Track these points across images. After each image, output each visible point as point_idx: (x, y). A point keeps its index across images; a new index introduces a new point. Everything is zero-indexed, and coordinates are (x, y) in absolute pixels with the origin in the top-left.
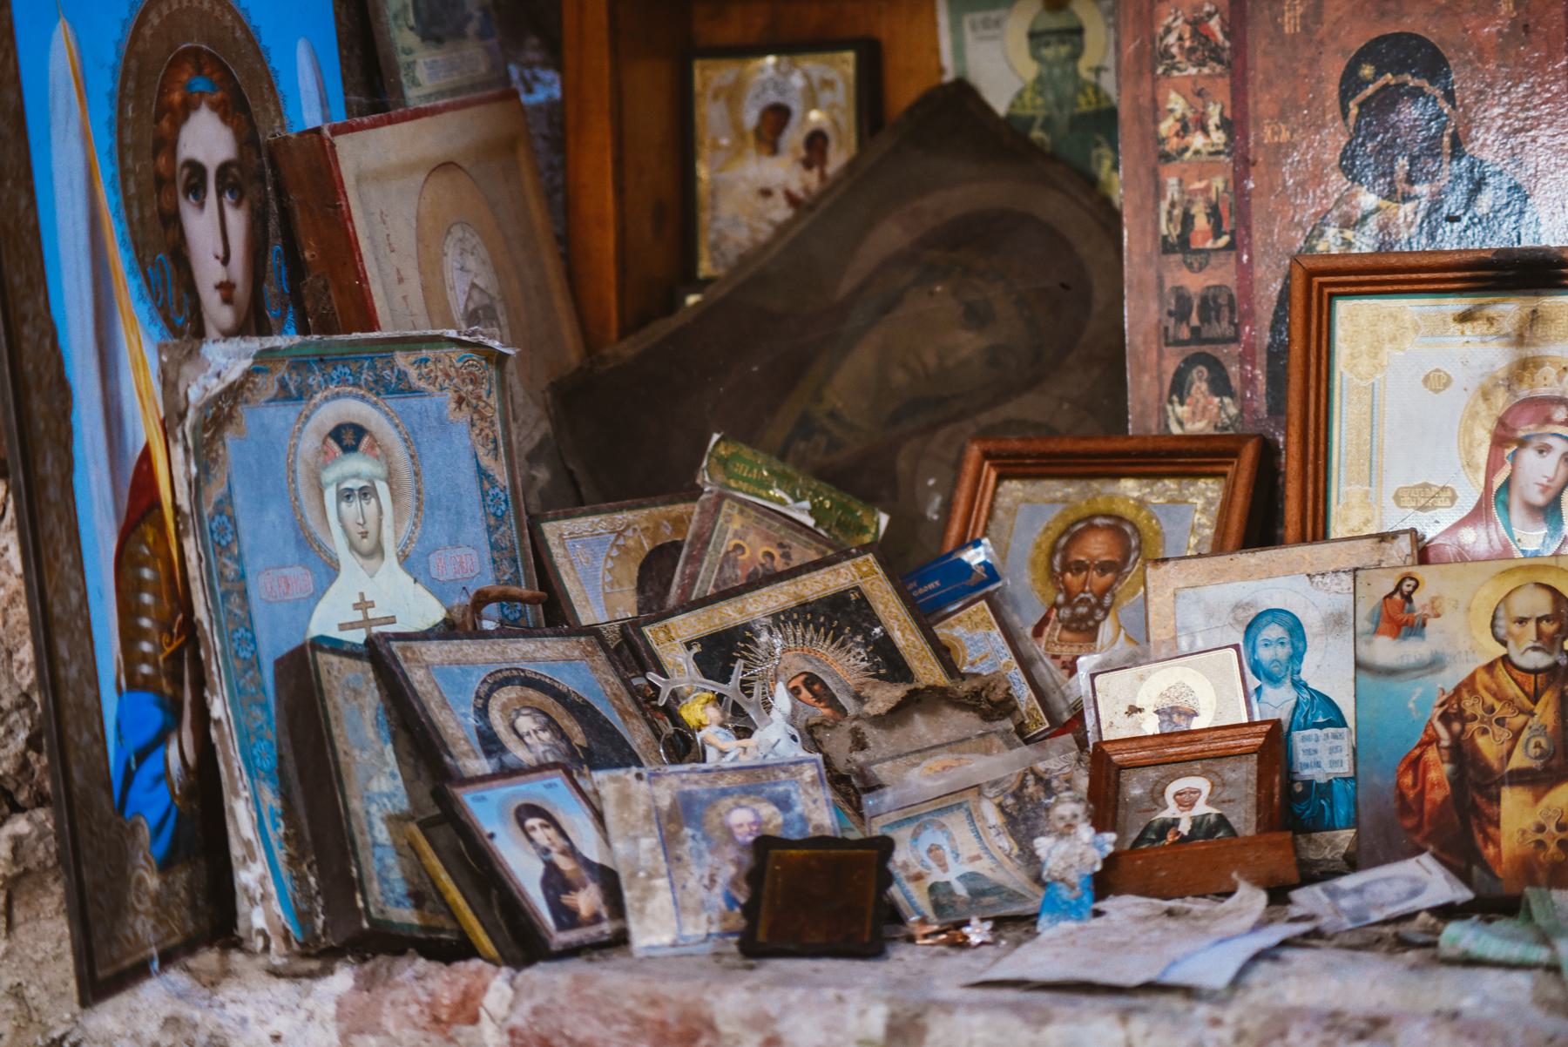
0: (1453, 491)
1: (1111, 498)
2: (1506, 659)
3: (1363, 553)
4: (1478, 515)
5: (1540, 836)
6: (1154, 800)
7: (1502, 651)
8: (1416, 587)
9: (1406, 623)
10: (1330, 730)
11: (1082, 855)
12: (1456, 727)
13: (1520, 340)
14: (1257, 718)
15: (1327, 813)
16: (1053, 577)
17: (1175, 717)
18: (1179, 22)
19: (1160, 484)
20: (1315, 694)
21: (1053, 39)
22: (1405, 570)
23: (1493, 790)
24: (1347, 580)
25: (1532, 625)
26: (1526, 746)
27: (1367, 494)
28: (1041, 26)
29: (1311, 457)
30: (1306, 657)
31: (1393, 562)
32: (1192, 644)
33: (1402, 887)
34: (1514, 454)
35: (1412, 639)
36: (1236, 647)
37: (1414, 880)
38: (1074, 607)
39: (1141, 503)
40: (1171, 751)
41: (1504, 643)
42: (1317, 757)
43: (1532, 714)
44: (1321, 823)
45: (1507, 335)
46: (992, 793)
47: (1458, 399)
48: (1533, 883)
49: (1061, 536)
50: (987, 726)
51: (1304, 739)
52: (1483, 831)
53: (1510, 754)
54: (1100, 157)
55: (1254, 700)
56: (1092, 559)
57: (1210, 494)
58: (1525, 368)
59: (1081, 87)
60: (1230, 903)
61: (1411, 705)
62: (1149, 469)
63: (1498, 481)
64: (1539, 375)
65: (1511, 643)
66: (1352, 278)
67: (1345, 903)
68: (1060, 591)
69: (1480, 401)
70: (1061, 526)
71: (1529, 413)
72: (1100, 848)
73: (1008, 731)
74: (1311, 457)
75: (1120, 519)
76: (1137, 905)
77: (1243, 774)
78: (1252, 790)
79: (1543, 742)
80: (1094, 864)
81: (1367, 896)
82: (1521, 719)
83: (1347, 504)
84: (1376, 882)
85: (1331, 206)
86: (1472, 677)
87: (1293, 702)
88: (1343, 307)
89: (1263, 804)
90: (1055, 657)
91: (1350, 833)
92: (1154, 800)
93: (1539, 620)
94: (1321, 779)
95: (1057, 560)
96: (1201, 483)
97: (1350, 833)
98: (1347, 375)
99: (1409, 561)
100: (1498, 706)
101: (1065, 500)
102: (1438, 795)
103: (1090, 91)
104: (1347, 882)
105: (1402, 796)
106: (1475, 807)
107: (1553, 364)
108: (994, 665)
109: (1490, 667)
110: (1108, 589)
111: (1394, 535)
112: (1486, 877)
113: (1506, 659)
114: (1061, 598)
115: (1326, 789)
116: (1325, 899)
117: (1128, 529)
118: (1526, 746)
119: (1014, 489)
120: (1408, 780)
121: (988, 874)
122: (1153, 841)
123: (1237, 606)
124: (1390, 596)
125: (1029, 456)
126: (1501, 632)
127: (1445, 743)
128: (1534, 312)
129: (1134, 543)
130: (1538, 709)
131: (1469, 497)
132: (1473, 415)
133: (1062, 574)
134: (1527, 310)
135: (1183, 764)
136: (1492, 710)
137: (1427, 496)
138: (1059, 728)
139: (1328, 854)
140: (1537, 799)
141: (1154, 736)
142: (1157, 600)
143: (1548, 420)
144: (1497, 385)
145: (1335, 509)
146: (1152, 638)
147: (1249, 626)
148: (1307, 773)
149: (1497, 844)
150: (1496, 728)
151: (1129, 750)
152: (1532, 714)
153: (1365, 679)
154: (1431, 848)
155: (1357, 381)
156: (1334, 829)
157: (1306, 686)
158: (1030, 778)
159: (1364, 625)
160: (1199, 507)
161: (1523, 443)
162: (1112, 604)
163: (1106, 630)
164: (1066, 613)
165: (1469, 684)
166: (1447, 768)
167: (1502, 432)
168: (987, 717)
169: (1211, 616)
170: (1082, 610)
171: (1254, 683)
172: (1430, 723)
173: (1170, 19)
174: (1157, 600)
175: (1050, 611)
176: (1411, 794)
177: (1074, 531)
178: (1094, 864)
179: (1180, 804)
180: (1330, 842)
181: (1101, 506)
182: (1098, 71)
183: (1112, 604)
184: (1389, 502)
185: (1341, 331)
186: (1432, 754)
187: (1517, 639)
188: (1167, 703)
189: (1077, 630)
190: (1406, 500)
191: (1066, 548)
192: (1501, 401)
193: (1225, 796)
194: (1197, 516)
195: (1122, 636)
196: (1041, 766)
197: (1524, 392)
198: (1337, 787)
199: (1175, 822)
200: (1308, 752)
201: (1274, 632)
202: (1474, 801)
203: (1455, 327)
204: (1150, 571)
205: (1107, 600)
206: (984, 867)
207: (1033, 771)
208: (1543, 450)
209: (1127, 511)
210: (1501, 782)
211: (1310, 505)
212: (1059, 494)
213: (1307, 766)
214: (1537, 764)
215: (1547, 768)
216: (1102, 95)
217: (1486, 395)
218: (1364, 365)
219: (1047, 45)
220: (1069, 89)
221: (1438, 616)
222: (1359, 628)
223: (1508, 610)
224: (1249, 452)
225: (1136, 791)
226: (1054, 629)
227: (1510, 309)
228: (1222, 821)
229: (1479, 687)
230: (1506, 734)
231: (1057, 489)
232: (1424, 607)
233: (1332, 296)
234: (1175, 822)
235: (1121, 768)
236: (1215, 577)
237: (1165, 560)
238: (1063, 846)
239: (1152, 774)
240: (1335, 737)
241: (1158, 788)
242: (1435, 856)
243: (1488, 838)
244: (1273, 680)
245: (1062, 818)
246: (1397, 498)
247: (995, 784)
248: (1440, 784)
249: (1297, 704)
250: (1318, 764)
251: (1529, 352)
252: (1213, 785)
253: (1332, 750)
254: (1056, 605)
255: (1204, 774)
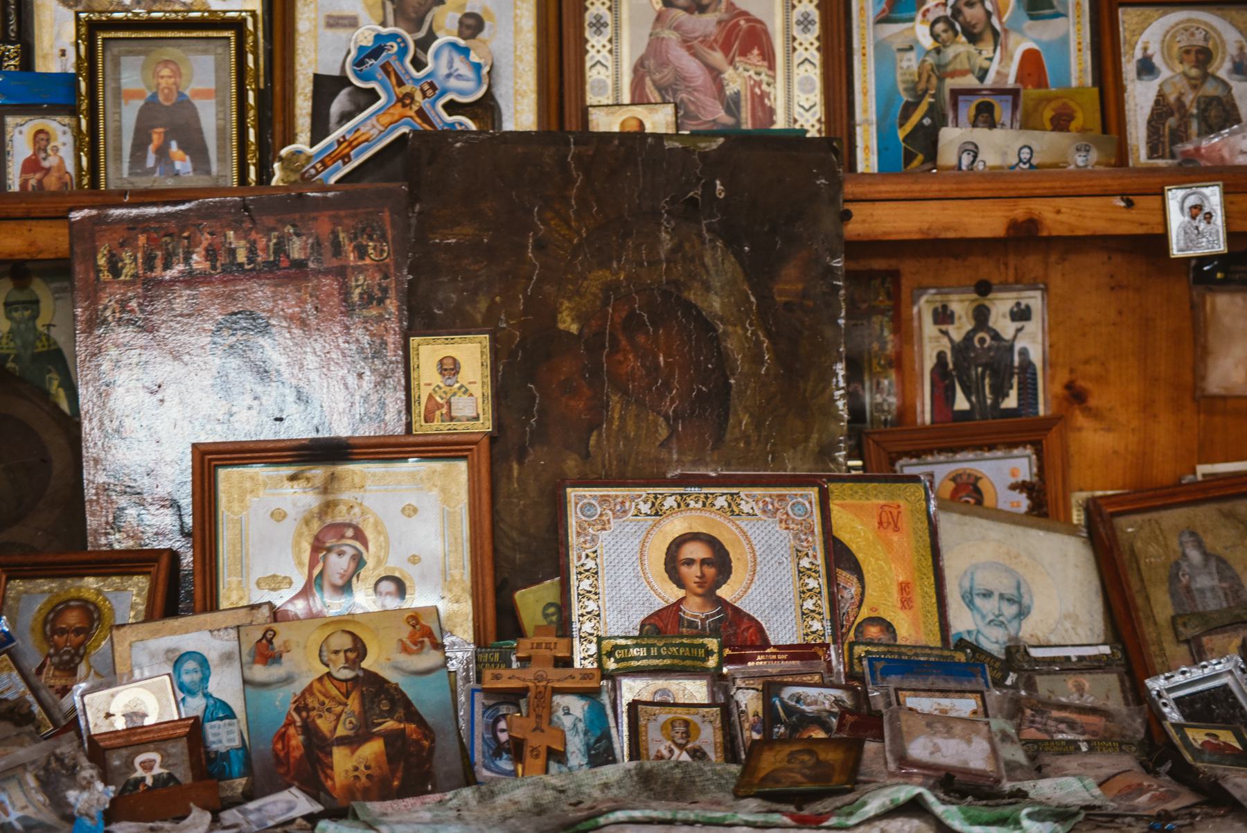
0: (290, 579)
1: (79, 589)
2: (329, 674)
3: (242, 617)
4: (305, 593)
5: (356, 773)
6: (128, 767)
7: (326, 670)
8: (275, 635)
9: (270, 656)
10: (227, 721)
11: (98, 800)
12: (304, 714)
13: (325, 490)
14: (184, 716)
15: (227, 769)
16: (47, 639)
17: (135, 718)
18: (112, 303)
19: (110, 580)
20: (217, 700)
21: (20, 306)
22: (268, 626)
23: (328, 749)
24: (233, 633)
25: (342, 654)
26: (344, 723)
27: (240, 582)
28: (11, 299)
29: (207, 561)
30: (211, 679)
31: (260, 621)
32: (142, 674)
33: (282, 806)
34: (325, 557)
35: (275, 665)
36: (169, 675)
37: (289, 802)
38: (61, 656)
39: (99, 592)
40: (136, 738)
41: (327, 666)
42: (220, 737)
43: (346, 705)
44: (224, 775)
45: (318, 488)
46: (30, 768)
47: (289, 527)
48: (354, 799)
49: (49, 613)
50: (19, 730)
51: (212, 727)
52: (324, 772)
53: (335, 728)
54: (50, 379)
55: (181, 705)
56: (70, 626)
57: (140, 585)
58: (328, 507)
59: (38, 337)
60: (187, 822)
61: (277, 703)
62: (103, 571)
63: (316, 572)
64: (337, 511)
65: (331, 665)
66: (228, 456)
67: (252, 817)
68: (51, 647)
69: (304, 526)
70: (49, 607)
71: (332, 533)
72: (107, 794)
73: (31, 732)
74: (207, 561)
75: (86, 601)
76: (131, 827)
77: (180, 749)
78: (186, 758)
79: (353, 720)
80: (104, 804)
81: (264, 813)
82: (339, 709)
83: (229, 589)
84: (270, 803)
85: (1179, 549)
86: (311, 685)
87: (204, 706)
88: (222, 473)
89: (193, 767)
90: (51, 687)
91: (243, 781)
92: (128, 767)
93: (346, 651)
94: (223, 750)
95: (48, 627)
96: (135, 578)
97: (243, 781)
98: (226, 513)
99: (269, 620)
100: (327, 701)
101: (51, 591)
102: (297, 754)
103: (44, 338)
104: (251, 806)
105: (276, 755)
106: (319, 760)
107: (344, 504)
108: (16, 692)
109: (320, 679)
110: (82, 644)
111: (259, 606)
112: (328, 798)
113: (329, 674)
114: (52, 651)
115: (226, 756)
116: (240, 816)
117: (92, 607)
118: (344, 723)
119: (18, 585)
120: (279, 746)
121: (33, 816)
122: (131, 791)
123: (169, 651)
124: (260, 641)
125: (27, 565)
126: (325, 659)
127: (299, 724)
128: (333, 474)
129: (96, 616)
130: (349, 702)
131: (299, 583)
132: (300, 535)
133: (52, 636)
134: (329, 473)
135: (143, 745)
136: (323, 704)
137: (275, 582)
138: (65, 729)
139: (229, 793)
140: (353, 752)
141: (123, 730)
142: (120, 649)
143: (343, 537)
144: (313, 517)
145: (222, 592)
146: (118, 671)
147: (176, 662)
148: (214, 747)
149: (332, 779)
150: (326, 713)
151: (110, 739)
152: (346, 705)
153: (249, 689)
154: (296, 783)
155: (232, 516)
156: (232, 778)
157: (211, 696)
158: (52, 758)
159: (246, 658)
160: (135, 592)
161: (329, 550)
162: (85, 653)
163: (82, 669)
164: (56, 660)
165: (309, 690)
166: (301, 738)
167: (317, 544)
168: (18, 724)
169: (153, 657)
170: (66, 657)
171: (180, 695)
172: (289, 713)
173: (107, 300)
174: (120, 649)
175: (45, 660)
176: (282, 754)
177: (56, 611)
178: (104, 804)
179: (144, 768)
180: (230, 786)
181: (73, 593)
182: (49, 326)
183: (85, 653)
184: (253, 586)
185: (222, 486)
186: (292, 731)
187: (335, 663)
188: (129, 710)
189: (64, 670)
190: (262, 584)
191: (54, 620)
192: (316, 526)
193: (170, 762)
194: (134, 598)
195: (92, 672)
196: (58, 751)
197: (329, 521)
198: (232, 754)
199: (143, 779)
200: (215, 735)
201: (190, 665)
202: (318, 757)
203: (287, 484)
204: (114, 632)
205: (82, 651)
206: (30, 812)
207: (54, 754)
208: (341, 554)
209: (90, 596)
210: (332, 745)
211: (208, 589)
212: (46, 588)
213: (214, 743)
214: (351, 733)
215: (357, 735)
216: (52, 341)
217: (307, 522)
218: (236, 506)
219: (16, 310)
220: (31, 337)
221: (288, 651)
222: (244, 660)
223: (328, 647)
224: (164, 560)
225: (117, 763)
226: (49, 670)
227: (318, 473)
228: (171, 777)
229: (316, 691)
230: (333, 717)
231: (46, 585)
232: (280, 646)
233: (216, 466)
234: (143, 779)
235: (106, 749)
236: (156, 634)
237: (123, 625)
238: (85, 795)
239: (124, 752)
240: (230, 725)
241: (130, 760)
242: (299, 788)
243: (328, 777)
244: (191, 693)
245: (85, 778)
246: (258, 584)
247: (33, 763)
248: (298, 747)
249: (207, 707)
250: (220, 741)
251: (331, 497)
252: (162, 756)
253: (229, 733)
254: (49, 655)
255: (156, 750)
